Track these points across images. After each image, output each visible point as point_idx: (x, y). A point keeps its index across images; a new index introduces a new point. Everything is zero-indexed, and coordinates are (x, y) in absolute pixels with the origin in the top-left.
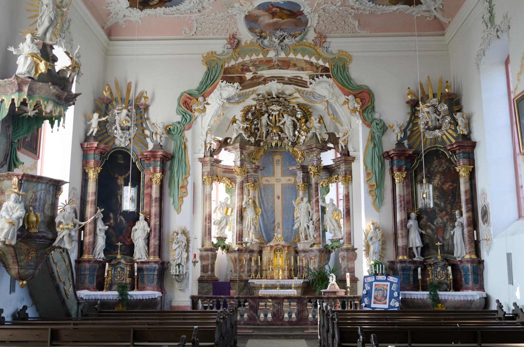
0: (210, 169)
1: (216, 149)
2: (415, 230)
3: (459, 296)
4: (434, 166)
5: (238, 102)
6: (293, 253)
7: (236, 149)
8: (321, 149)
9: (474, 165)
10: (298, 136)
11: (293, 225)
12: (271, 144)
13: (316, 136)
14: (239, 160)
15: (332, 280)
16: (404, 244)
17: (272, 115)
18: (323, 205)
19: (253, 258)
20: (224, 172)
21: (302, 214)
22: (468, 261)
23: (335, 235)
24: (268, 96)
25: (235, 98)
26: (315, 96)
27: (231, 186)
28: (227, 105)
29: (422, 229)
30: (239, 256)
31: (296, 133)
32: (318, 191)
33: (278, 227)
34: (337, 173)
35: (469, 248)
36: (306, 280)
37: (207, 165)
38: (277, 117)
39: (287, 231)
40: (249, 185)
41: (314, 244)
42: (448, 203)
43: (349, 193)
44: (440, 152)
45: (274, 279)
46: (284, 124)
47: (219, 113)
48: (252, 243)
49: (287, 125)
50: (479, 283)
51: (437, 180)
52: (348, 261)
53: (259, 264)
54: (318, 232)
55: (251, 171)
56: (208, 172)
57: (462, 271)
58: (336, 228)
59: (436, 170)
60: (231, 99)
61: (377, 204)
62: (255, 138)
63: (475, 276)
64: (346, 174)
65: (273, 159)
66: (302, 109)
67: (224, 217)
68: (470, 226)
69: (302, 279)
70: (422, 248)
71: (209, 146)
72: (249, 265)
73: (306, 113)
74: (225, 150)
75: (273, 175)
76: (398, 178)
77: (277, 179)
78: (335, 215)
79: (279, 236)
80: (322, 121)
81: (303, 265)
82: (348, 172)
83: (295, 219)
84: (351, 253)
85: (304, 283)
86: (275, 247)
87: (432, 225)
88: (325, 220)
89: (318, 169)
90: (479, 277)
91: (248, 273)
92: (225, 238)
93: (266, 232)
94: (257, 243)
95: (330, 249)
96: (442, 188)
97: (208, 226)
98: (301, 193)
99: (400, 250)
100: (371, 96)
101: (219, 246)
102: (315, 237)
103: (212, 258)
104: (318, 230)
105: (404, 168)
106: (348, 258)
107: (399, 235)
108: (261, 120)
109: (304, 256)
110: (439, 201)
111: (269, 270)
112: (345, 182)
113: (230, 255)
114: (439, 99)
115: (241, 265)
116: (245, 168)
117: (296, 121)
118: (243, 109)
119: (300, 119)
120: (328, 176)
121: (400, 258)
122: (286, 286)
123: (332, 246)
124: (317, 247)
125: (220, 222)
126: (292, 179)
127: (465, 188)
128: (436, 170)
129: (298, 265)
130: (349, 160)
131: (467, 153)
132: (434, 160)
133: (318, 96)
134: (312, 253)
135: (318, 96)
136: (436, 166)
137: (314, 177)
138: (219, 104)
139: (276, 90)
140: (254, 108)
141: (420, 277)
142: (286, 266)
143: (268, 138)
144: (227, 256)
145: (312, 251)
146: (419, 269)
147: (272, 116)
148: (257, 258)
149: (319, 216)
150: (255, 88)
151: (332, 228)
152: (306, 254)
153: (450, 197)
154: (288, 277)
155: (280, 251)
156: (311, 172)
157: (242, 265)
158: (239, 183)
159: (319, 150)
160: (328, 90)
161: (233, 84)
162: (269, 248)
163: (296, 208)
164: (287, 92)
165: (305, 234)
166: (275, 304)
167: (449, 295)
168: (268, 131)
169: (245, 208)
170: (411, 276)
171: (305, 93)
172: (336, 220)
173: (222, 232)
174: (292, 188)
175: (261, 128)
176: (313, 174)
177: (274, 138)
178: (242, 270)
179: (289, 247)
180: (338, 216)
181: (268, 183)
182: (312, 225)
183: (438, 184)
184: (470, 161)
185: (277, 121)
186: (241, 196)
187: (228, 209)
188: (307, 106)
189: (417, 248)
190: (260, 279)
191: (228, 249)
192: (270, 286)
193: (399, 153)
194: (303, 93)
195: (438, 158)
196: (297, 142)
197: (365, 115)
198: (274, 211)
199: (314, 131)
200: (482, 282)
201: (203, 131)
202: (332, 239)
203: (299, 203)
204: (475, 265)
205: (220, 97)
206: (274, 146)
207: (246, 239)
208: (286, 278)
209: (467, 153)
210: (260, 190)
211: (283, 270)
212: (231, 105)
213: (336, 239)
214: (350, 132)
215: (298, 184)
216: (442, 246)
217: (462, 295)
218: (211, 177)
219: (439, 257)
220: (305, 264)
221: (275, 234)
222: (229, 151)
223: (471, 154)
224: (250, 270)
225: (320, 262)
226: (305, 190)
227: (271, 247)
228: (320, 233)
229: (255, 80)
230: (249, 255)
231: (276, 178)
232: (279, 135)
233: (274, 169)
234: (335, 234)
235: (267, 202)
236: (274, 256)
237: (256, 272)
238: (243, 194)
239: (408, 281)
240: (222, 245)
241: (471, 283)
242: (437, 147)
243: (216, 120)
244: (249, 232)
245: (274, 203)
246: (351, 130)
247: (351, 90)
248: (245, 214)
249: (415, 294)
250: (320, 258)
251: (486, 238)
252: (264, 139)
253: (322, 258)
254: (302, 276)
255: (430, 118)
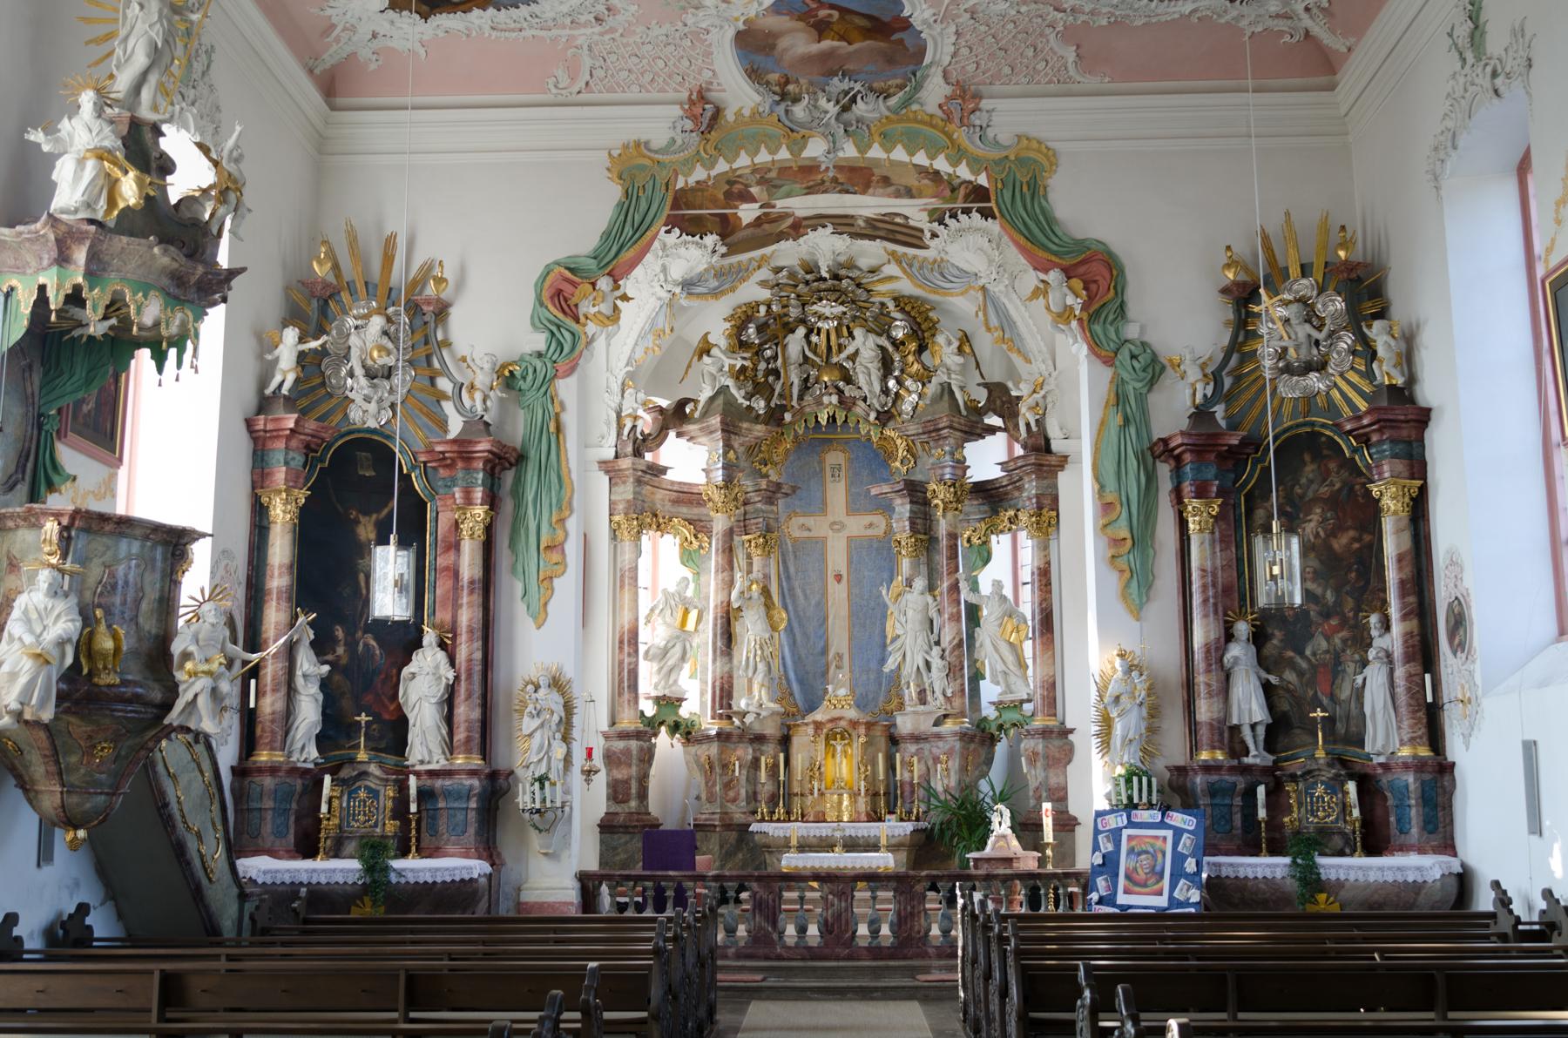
0: (635, 493)
1: (650, 435)
2: (1247, 671)
3: (1381, 869)
4: (1303, 481)
5: (716, 294)
6: (882, 742)
7: (711, 433)
8: (966, 432)
9: (1424, 478)
10: (897, 394)
11: (883, 661)
12: (816, 417)
13: (951, 393)
14: (720, 465)
15: (1000, 823)
16: (1215, 716)
17: (819, 330)
18: (973, 599)
19: (763, 759)
20: (676, 502)
21: (909, 626)
22: (1406, 766)
23: (1008, 689)
24: (807, 273)
25: (706, 281)
26: (946, 272)
27: (696, 544)
28: (684, 302)
29: (1268, 672)
30: (721, 752)
31: (892, 383)
32: (957, 557)
33: (838, 667)
34: (1012, 502)
35: (1411, 727)
36: (923, 825)
37: (624, 482)
38: (833, 337)
39: (864, 677)
40: (750, 541)
41: (945, 716)
42: (1347, 593)
43: (1048, 563)
44: (1323, 439)
45: (825, 821)
46: (853, 357)
47: (661, 326)
48: (758, 714)
49: (863, 361)
50: (1441, 829)
51: (1312, 524)
52: (1047, 767)
53: (782, 778)
54: (959, 681)
55: (757, 499)
56: (628, 501)
57: (1389, 795)
58: (1012, 667)
59: (1310, 494)
60: (694, 285)
61: (1135, 596)
62: (768, 401)
63: (1427, 810)
64: (1040, 507)
65: (821, 462)
66: (908, 313)
67: (678, 637)
68: (1414, 660)
69: (909, 820)
70: (1269, 728)
71: (629, 424)
72: (753, 780)
73: (919, 324)
74: (679, 435)
75: (823, 509)
76: (1197, 518)
77: (834, 523)
78: (1009, 628)
79: (842, 692)
80: (967, 349)
81: (912, 778)
82: (1047, 501)
83: (888, 641)
84: (1057, 743)
85: (915, 831)
86: (829, 726)
87: (1298, 660)
88: (977, 645)
89: (955, 493)
90: (1440, 814)
91: (748, 803)
92: (681, 700)
93: (801, 682)
94: (774, 713)
95: (993, 730)
96: (1330, 548)
97: (630, 664)
98: (905, 565)
99: (1204, 733)
100: (1115, 273)
101: (661, 723)
102: (949, 695)
103: (641, 761)
104: (958, 674)
105: (1215, 489)
106: (1047, 757)
107: (1201, 689)
108: (785, 347)
109: (918, 752)
110: (1319, 585)
111: (812, 794)
112: (1039, 529)
113: (693, 749)
114: (1320, 280)
115: (726, 779)
116: (737, 490)
117: (890, 349)
118: (731, 312)
119: (903, 343)
120: (986, 512)
121: (1204, 756)
122: (861, 842)
123: (1000, 721)
124: (955, 724)
125: (665, 652)
126: (880, 521)
127: (1398, 545)
128: (1310, 494)
129: (898, 778)
130: (1050, 466)
131: (1405, 442)
132: (1305, 464)
133: (956, 272)
134: (941, 744)
135: (956, 272)
136: (1311, 482)
137: (944, 516)
138: (660, 299)
139: (829, 256)
140: (763, 309)
141: (1262, 813)
142: (863, 783)
143: (808, 398)
144: (685, 752)
145: (938, 736)
146: (1261, 790)
147: (818, 334)
148: (776, 757)
149: (959, 632)
150: (768, 250)
151: (1000, 667)
152: (922, 746)
153: (1353, 575)
154: (868, 815)
155: (843, 738)
156: (936, 501)
157: (732, 780)
158: (720, 535)
159: (958, 434)
160: (985, 253)
161: (701, 238)
162: (810, 730)
163: (892, 608)
164: (864, 263)
165: (918, 686)
166: (830, 897)
167: (1350, 867)
168: (806, 380)
169: (739, 609)
170: (1235, 809)
171: (916, 264)
172: (1011, 644)
173: (671, 682)
174: (877, 550)
175: (786, 371)
176: (941, 506)
177: (826, 399)
178: (731, 794)
179: (869, 726)
180: (1018, 632)
181: (806, 534)
182: (939, 661)
183: (1317, 535)
184: (1411, 467)
185: (834, 349)
186: (725, 574)
187: (686, 612)
188: (922, 305)
189: (1253, 727)
190: (784, 821)
191: (689, 733)
192: (814, 841)
193: (1200, 442)
194: (911, 266)
195: (1317, 456)
196: (893, 410)
197: (1097, 328)
198: (826, 619)
199: (945, 378)
200: (1448, 828)
201: (612, 379)
202: (1001, 703)
203: (899, 595)
204: (1427, 777)
205: (662, 277)
206: (824, 423)
207: (741, 703)
208: (863, 817)
209: (1405, 442)
210: (783, 555)
211: (854, 795)
212: (695, 303)
213: (1012, 702)
214: (1052, 380)
215: (898, 537)
216: (1330, 722)
217: (1390, 868)
218: (635, 516)
219: (1320, 754)
220: (919, 777)
221: (830, 688)
222: (691, 439)
223: (1415, 445)
224: (755, 793)
225: (963, 769)
226: (917, 556)
227: (818, 726)
228: (963, 685)
229: (766, 226)
230: (750, 751)
231: (830, 518)
232: (840, 392)
233: (824, 492)
234: (1008, 686)
235: (804, 591)
236: (826, 753)
237: (773, 800)
238: (732, 569)
239: (1228, 827)
240: (671, 720)
241: (1414, 831)
242: (1313, 424)
243: (651, 345)
244: (750, 681)
245: (824, 593)
246: (1054, 374)
247: (1055, 254)
248: (738, 628)
249: (1249, 865)
250: (964, 758)
251: (1460, 697)
252: (794, 403)
253: (970, 758)
254: (910, 812)
255: (1293, 337)
